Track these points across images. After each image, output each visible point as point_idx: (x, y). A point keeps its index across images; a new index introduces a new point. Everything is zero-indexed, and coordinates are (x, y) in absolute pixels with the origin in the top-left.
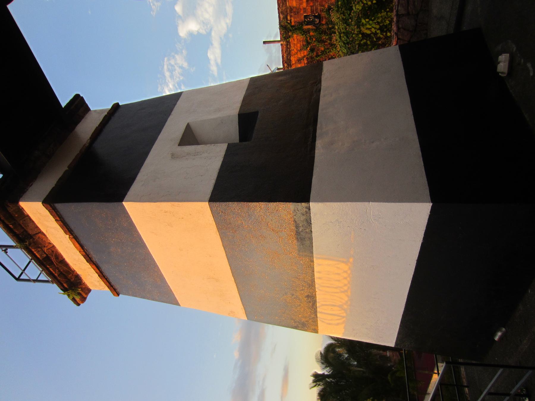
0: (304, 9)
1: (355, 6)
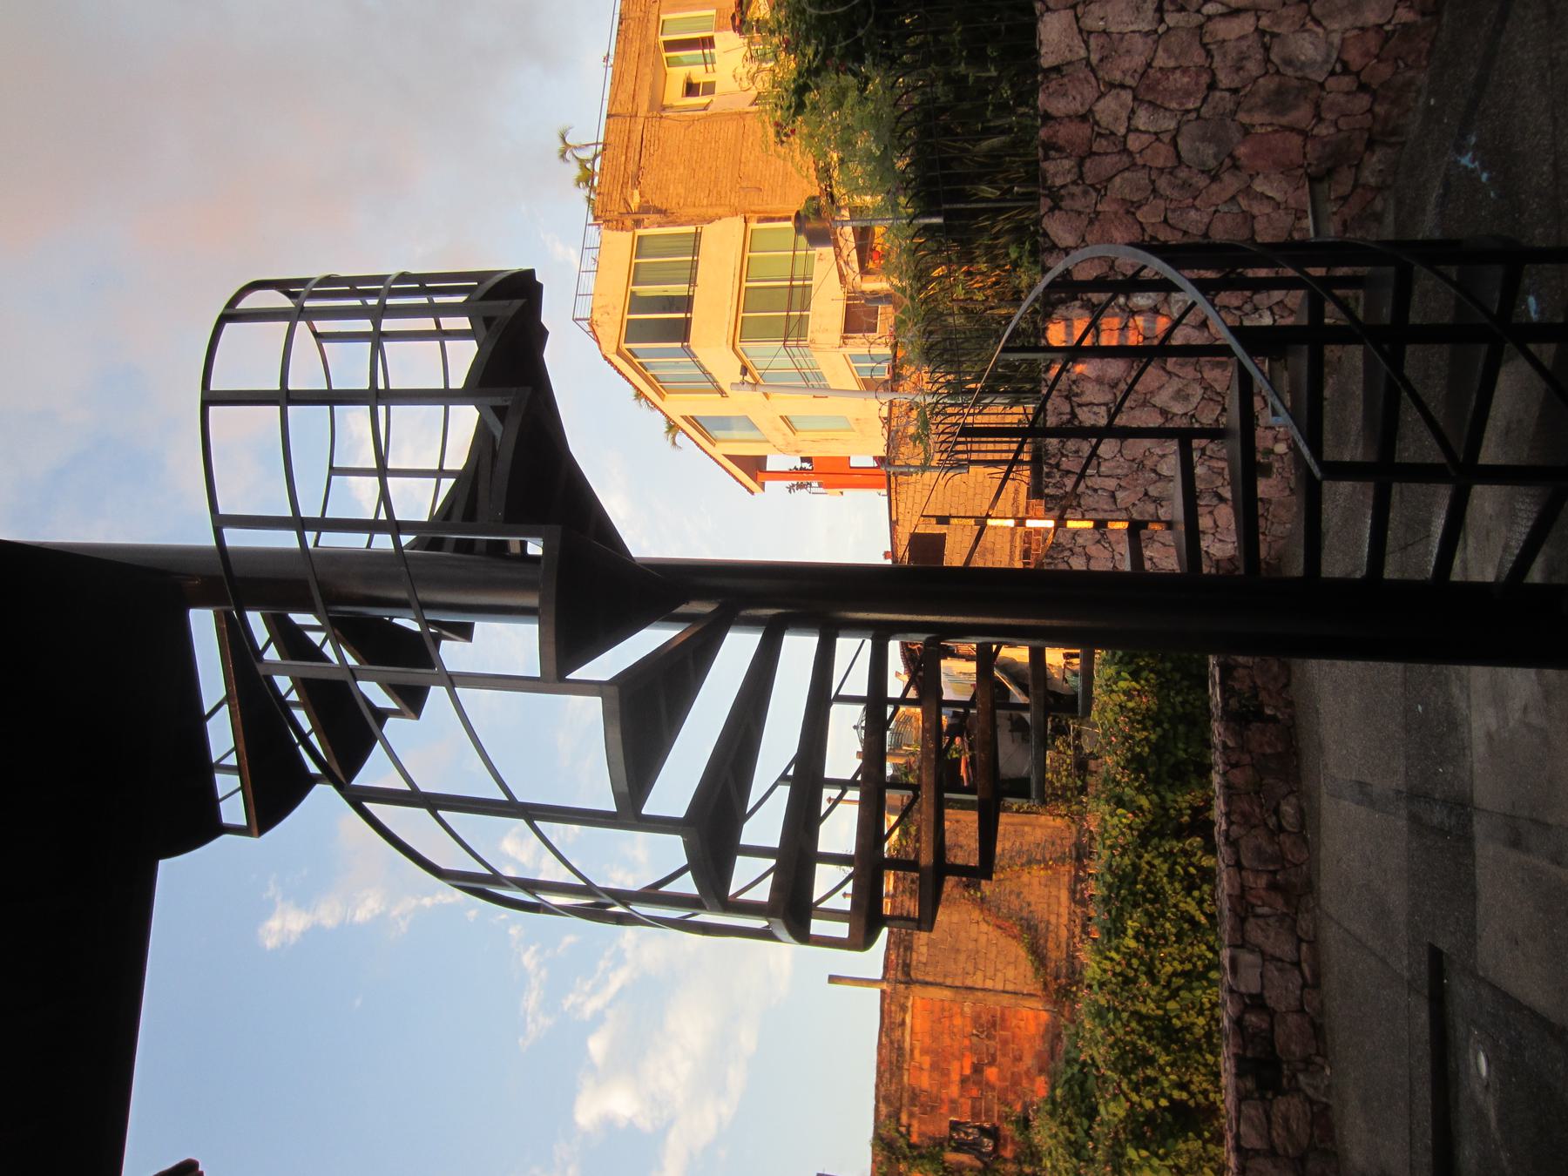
0: (952, 1101)
1: (1106, 1104)
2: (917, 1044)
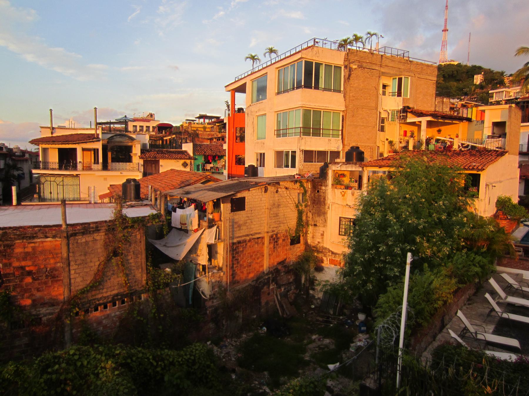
0: (10, 264)
2: (37, 245)
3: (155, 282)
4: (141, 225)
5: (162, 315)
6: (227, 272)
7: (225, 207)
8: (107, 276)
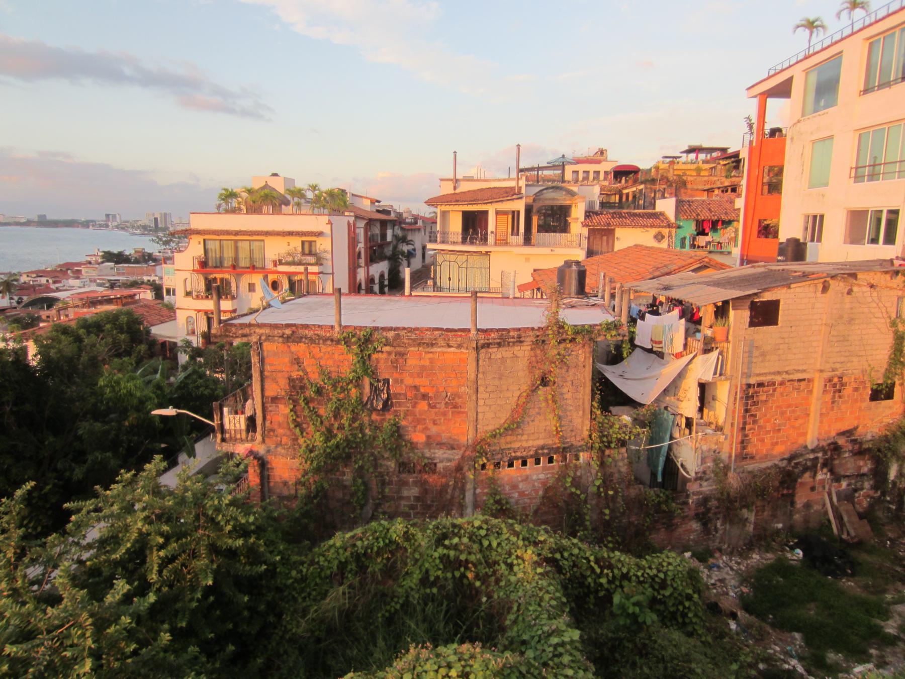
0: (402, 381)
3: (604, 436)
4: (587, 337)
5: (611, 493)
6: (732, 436)
7: (739, 317)
8: (529, 416)
